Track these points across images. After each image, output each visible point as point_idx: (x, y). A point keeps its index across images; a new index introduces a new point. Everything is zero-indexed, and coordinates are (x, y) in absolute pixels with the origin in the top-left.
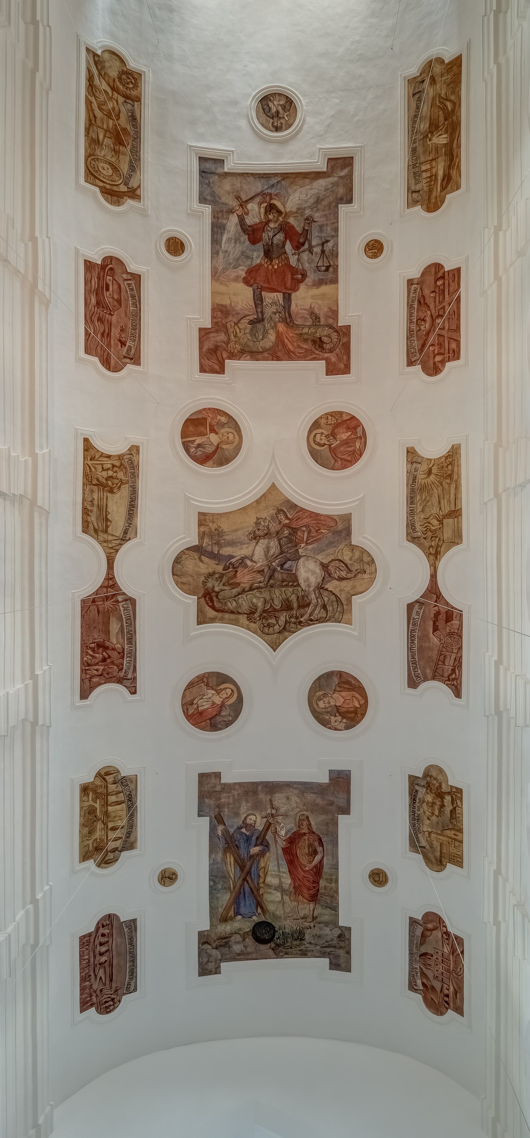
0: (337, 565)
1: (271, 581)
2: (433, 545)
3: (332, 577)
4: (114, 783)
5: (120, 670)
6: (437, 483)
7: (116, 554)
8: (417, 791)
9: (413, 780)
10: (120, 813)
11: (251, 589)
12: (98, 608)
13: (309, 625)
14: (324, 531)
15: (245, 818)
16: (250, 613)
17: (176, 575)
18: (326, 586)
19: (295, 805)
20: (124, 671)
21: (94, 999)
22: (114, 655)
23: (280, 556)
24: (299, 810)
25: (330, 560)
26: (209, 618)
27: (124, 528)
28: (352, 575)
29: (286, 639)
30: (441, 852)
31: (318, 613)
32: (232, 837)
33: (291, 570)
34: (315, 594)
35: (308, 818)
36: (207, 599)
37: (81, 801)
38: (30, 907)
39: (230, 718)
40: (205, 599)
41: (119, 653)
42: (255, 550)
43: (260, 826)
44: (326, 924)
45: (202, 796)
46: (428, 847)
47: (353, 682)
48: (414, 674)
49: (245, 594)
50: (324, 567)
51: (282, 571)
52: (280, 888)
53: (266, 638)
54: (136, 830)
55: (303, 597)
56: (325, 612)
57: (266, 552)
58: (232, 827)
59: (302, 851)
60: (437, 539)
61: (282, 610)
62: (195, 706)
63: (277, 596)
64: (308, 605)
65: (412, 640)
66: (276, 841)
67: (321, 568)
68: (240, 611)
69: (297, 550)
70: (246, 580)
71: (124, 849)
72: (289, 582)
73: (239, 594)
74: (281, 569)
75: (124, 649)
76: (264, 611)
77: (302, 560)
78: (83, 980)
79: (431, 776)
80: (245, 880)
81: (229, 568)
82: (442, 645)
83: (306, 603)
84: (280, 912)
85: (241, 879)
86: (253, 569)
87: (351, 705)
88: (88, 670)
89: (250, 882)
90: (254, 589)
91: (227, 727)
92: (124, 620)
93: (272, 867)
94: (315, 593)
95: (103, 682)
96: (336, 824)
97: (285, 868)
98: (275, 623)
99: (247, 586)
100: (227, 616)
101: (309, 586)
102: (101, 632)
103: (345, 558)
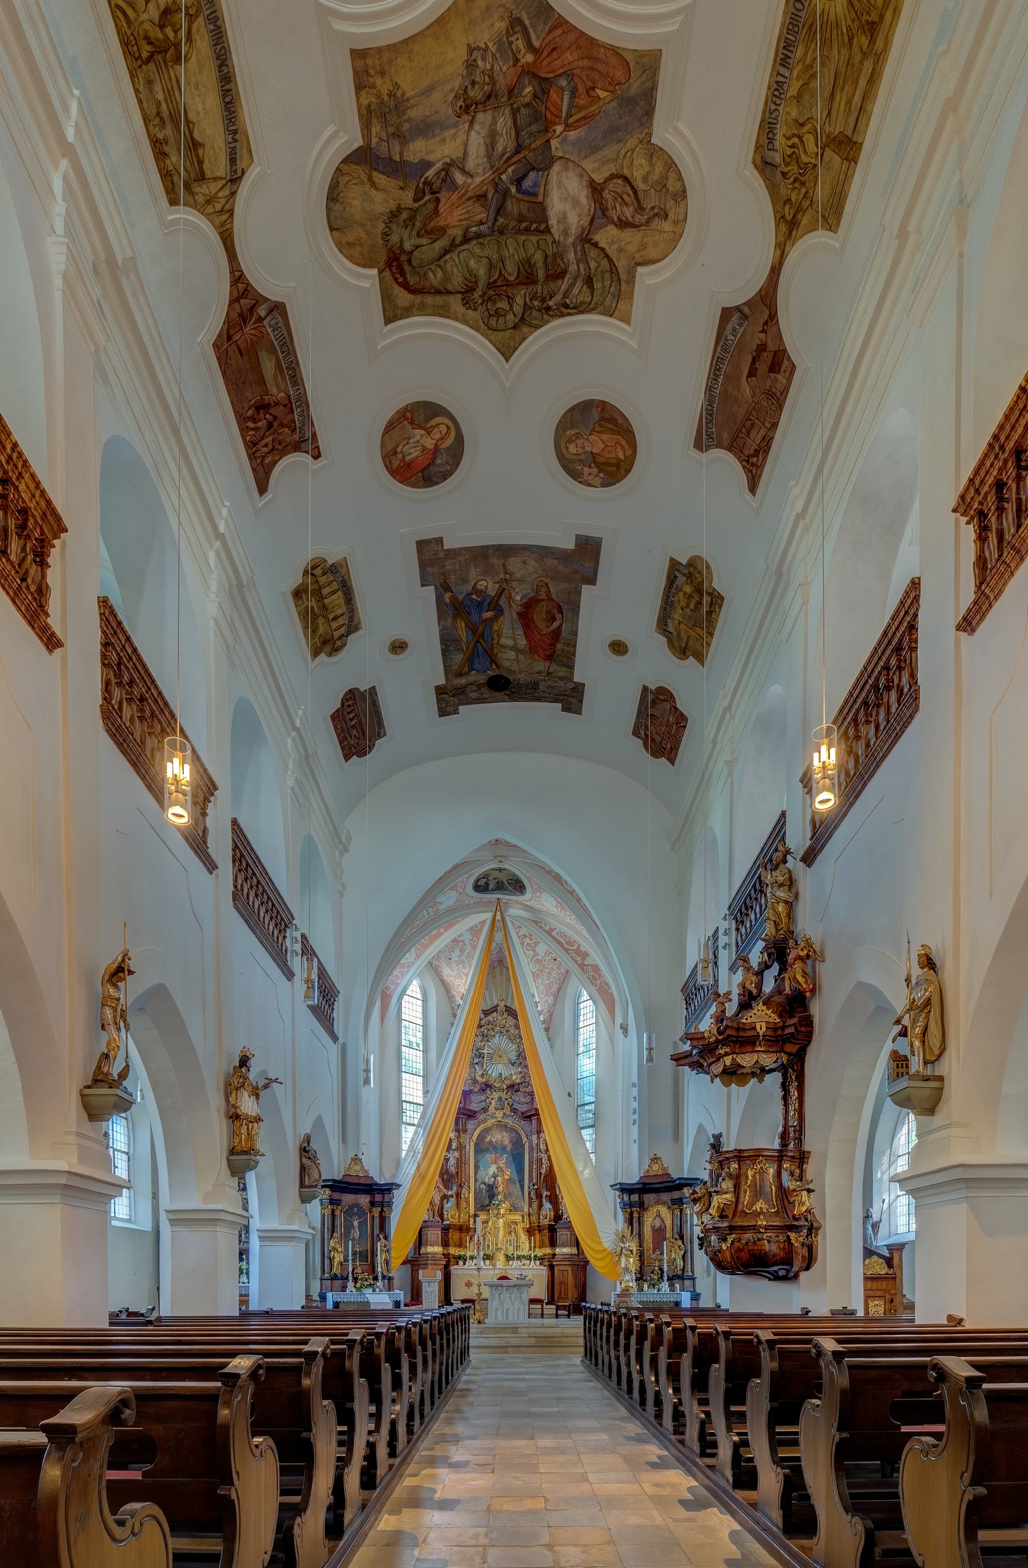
0: (619, 190)
1: (501, 220)
2: (793, 199)
3: (607, 218)
4: (324, 575)
5: (292, 432)
6: (844, 30)
7: (232, 222)
8: (676, 577)
9: (674, 564)
10: (337, 602)
11: (466, 240)
12: (238, 346)
13: (563, 315)
14: (602, 94)
15: (475, 584)
16: (467, 292)
17: (336, 229)
18: (597, 238)
19: (533, 570)
20: (298, 430)
21: (353, 750)
22: (279, 411)
23: (515, 159)
24: (536, 575)
25: (607, 175)
26: (402, 308)
27: (229, 150)
28: (643, 220)
29: (524, 339)
30: (687, 644)
31: (579, 293)
32: (461, 603)
33: (535, 195)
34: (575, 253)
35: (547, 585)
36: (394, 269)
37: (297, 606)
38: (294, 734)
39: (448, 467)
40: (391, 270)
41: (285, 406)
42: (470, 142)
43: (492, 590)
44: (561, 678)
45: (423, 565)
46: (675, 633)
47: (620, 421)
48: (706, 431)
49: (456, 252)
50: (596, 190)
51: (520, 196)
52: (515, 648)
53: (493, 338)
54: (358, 613)
55: (555, 255)
56: (589, 294)
57: (490, 149)
58: (461, 593)
59: (539, 617)
60: (803, 191)
61: (518, 284)
62: (400, 456)
63: (511, 252)
64: (562, 274)
65: (715, 374)
66: (510, 606)
67: (590, 195)
68: (450, 288)
69: (548, 141)
70: (456, 219)
71: (349, 633)
72: (531, 223)
73: (447, 251)
74: (518, 191)
75: (289, 397)
76: (490, 285)
77: (556, 167)
78: (341, 742)
79: (695, 568)
80: (478, 641)
81: (424, 195)
82: (753, 404)
83: (559, 270)
84: (514, 667)
85: (474, 642)
86: (467, 192)
87: (613, 455)
88: (256, 451)
89: (483, 642)
90: (471, 239)
91: (445, 480)
92: (278, 348)
93: (506, 630)
94: (575, 249)
95: (277, 458)
96: (579, 593)
97: (520, 632)
98: (508, 309)
99: (457, 232)
100: (430, 300)
101: (566, 233)
102: (253, 385)
103: (635, 174)
